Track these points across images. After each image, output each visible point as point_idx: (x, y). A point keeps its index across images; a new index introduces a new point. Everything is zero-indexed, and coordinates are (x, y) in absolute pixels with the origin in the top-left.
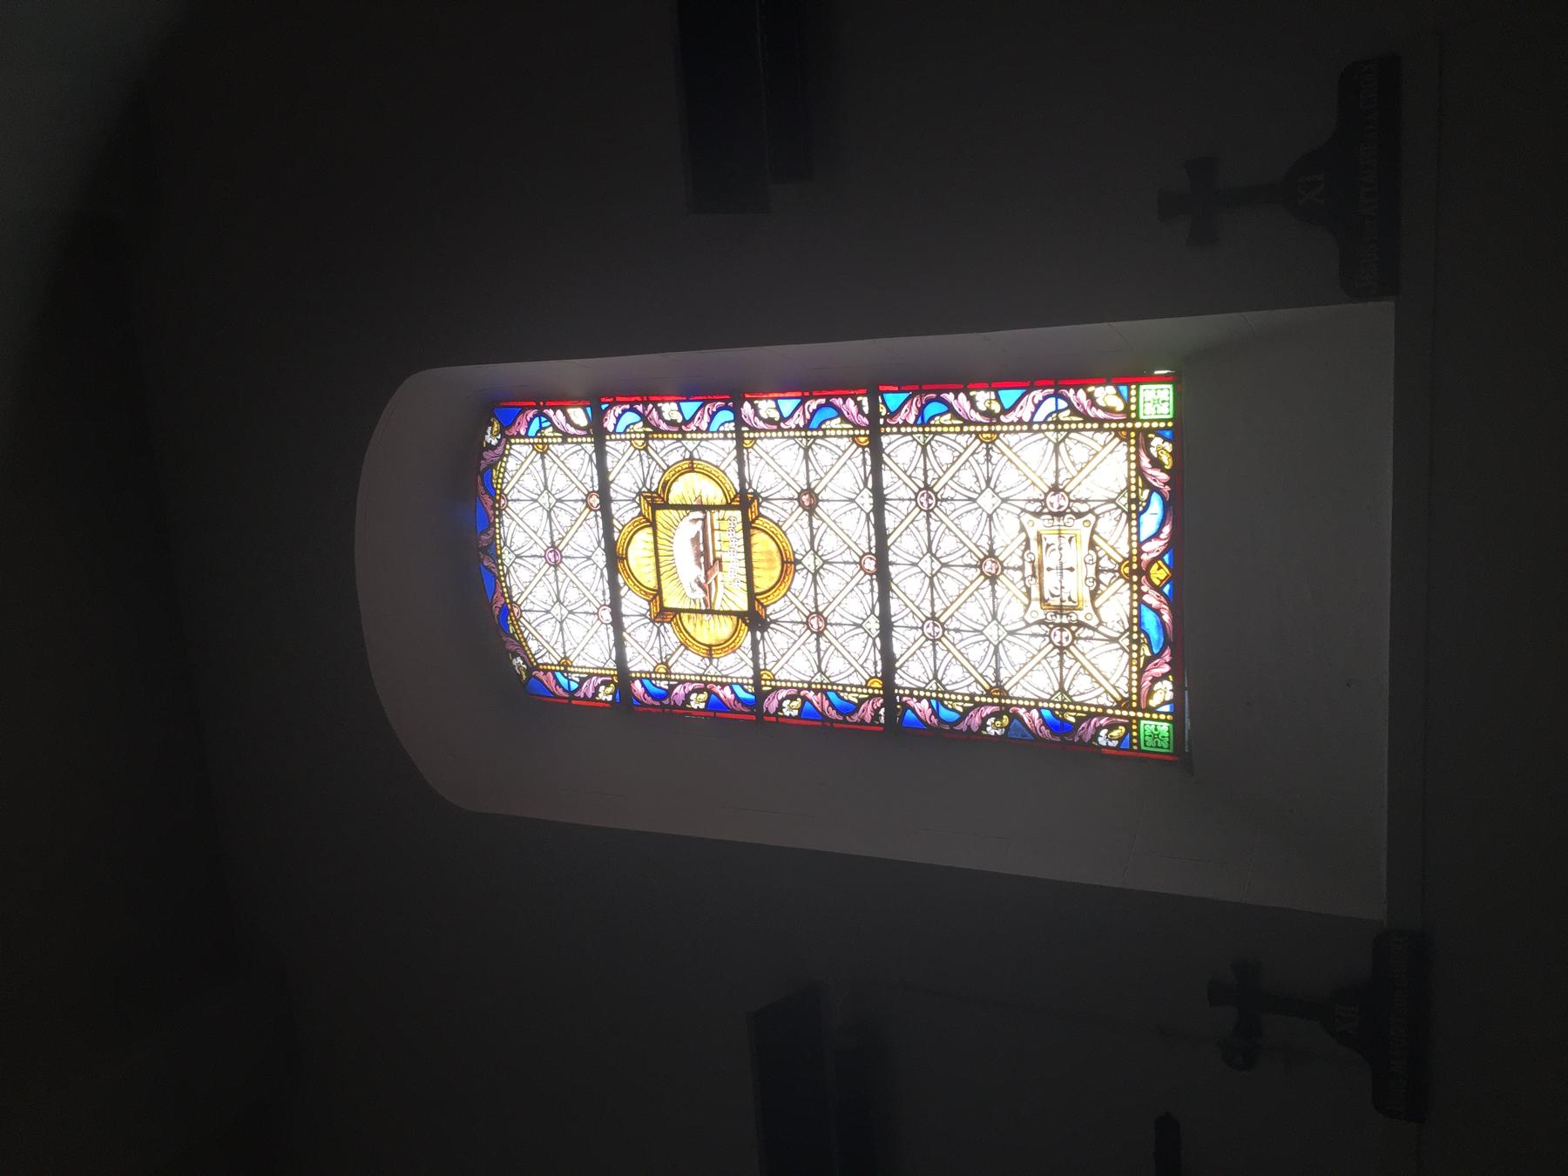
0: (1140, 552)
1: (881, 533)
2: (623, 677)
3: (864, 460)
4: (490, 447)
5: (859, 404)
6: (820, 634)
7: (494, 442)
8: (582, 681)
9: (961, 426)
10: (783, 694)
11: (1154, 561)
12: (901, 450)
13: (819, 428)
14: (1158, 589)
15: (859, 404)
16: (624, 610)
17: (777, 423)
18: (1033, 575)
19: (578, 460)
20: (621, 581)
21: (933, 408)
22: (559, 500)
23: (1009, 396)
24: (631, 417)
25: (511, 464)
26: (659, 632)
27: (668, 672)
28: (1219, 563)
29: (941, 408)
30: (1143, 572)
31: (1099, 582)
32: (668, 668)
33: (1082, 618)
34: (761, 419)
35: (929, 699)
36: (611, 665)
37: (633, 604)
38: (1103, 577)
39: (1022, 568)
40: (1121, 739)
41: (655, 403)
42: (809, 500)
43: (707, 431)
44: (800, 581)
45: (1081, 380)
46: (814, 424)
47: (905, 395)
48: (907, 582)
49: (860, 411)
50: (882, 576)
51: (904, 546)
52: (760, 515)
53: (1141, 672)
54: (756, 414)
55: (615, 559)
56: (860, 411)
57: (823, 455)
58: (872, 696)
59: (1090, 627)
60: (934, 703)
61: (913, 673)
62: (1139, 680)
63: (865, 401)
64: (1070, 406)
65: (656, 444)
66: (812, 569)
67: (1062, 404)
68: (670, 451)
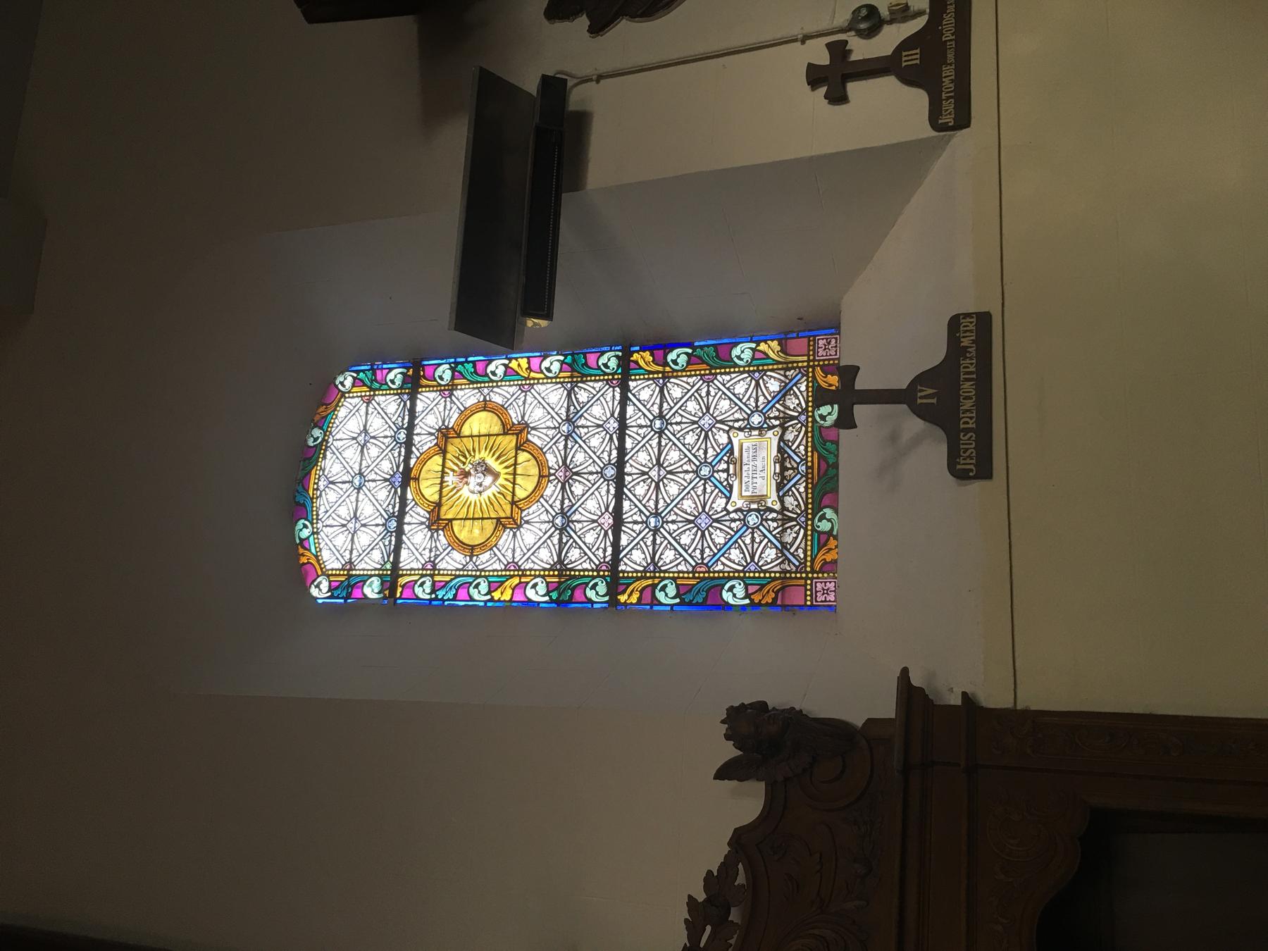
1: (622, 451)
2: (391, 577)
3: (608, 491)
19: (391, 404)
20: (409, 496)
22: (670, 472)
25: (342, 412)
26: (432, 536)
31: (784, 478)
33: (769, 505)
44: (551, 490)
46: (648, 593)
50: (619, 481)
51: (640, 459)
52: (528, 440)
59: (774, 511)
66: (562, 479)
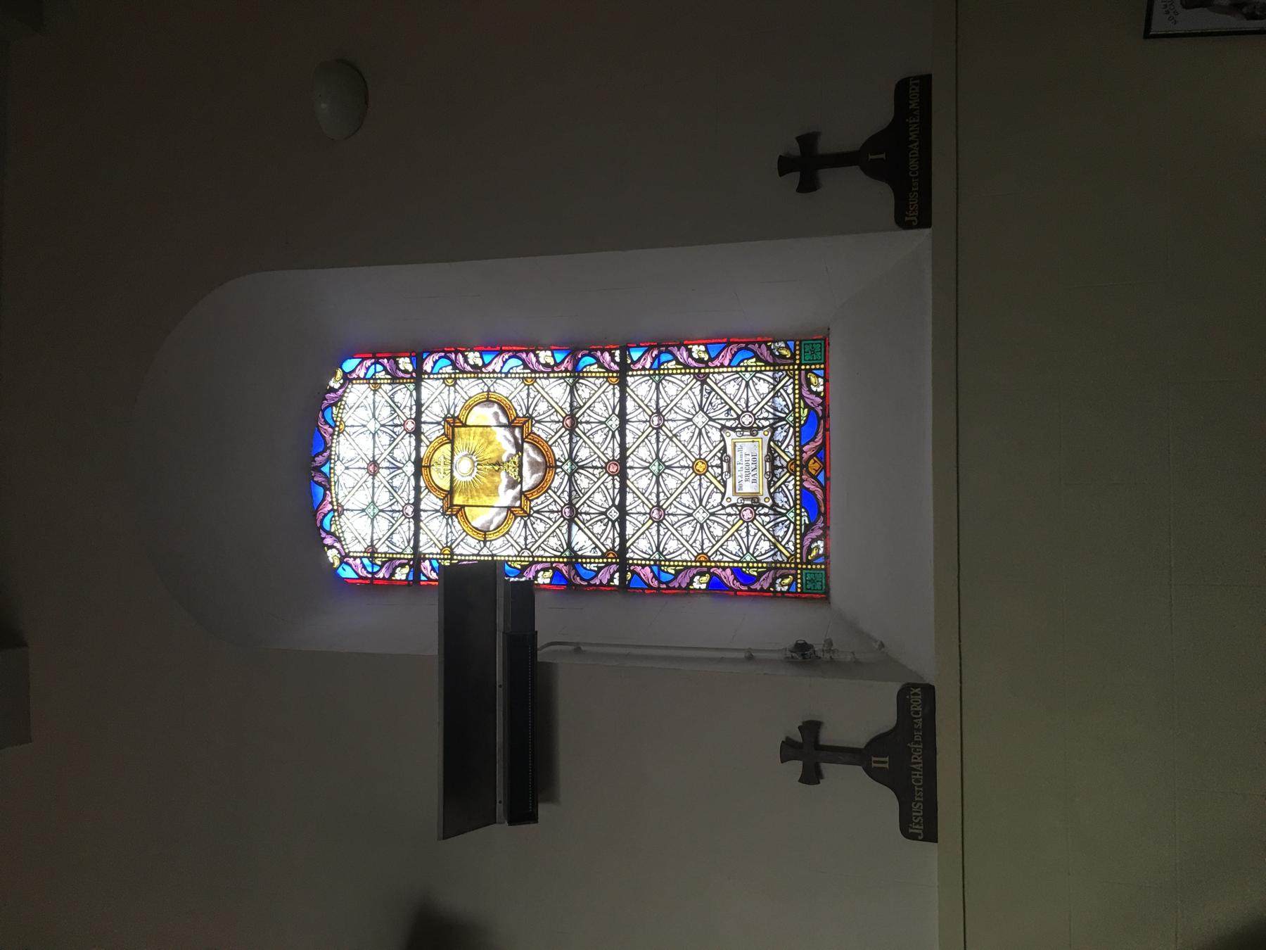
0: (802, 452)
4: (333, 390)
5: (612, 356)
6: (659, 523)
7: (337, 386)
8: (678, 573)
9: (548, 373)
10: (539, 567)
11: (811, 457)
12: (640, 387)
13: (738, 365)
14: (815, 477)
15: (612, 356)
16: (423, 506)
17: (552, 367)
18: (729, 471)
21: (664, 357)
23: (487, 358)
24: (514, 362)
27: (452, 554)
28: (813, 461)
29: (669, 357)
30: (804, 466)
32: (452, 550)
34: (694, 359)
35: (650, 566)
36: (409, 550)
37: (430, 502)
38: (778, 472)
39: (721, 467)
40: (790, 585)
41: (534, 352)
42: (572, 422)
43: (729, 366)
44: (559, 481)
45: (534, 348)
47: (358, 361)
48: (640, 481)
49: (613, 360)
51: (641, 454)
52: (532, 432)
53: (803, 536)
54: (538, 361)
55: (420, 466)
56: (613, 360)
57: (670, 388)
58: (608, 564)
60: (655, 569)
61: (641, 547)
62: (801, 543)
63: (617, 353)
64: (385, 369)
65: (462, 383)
67: (379, 368)
68: (472, 387)
